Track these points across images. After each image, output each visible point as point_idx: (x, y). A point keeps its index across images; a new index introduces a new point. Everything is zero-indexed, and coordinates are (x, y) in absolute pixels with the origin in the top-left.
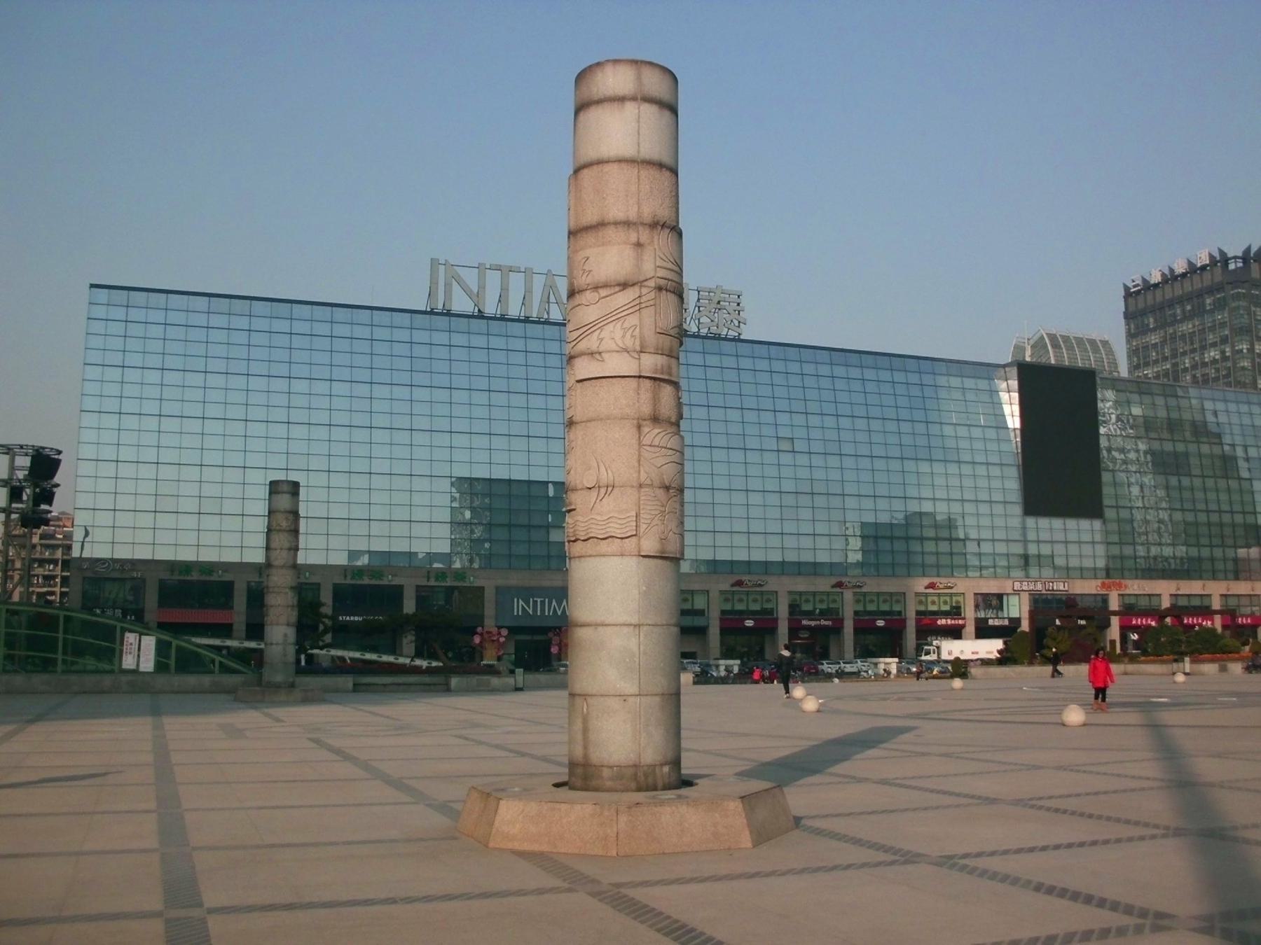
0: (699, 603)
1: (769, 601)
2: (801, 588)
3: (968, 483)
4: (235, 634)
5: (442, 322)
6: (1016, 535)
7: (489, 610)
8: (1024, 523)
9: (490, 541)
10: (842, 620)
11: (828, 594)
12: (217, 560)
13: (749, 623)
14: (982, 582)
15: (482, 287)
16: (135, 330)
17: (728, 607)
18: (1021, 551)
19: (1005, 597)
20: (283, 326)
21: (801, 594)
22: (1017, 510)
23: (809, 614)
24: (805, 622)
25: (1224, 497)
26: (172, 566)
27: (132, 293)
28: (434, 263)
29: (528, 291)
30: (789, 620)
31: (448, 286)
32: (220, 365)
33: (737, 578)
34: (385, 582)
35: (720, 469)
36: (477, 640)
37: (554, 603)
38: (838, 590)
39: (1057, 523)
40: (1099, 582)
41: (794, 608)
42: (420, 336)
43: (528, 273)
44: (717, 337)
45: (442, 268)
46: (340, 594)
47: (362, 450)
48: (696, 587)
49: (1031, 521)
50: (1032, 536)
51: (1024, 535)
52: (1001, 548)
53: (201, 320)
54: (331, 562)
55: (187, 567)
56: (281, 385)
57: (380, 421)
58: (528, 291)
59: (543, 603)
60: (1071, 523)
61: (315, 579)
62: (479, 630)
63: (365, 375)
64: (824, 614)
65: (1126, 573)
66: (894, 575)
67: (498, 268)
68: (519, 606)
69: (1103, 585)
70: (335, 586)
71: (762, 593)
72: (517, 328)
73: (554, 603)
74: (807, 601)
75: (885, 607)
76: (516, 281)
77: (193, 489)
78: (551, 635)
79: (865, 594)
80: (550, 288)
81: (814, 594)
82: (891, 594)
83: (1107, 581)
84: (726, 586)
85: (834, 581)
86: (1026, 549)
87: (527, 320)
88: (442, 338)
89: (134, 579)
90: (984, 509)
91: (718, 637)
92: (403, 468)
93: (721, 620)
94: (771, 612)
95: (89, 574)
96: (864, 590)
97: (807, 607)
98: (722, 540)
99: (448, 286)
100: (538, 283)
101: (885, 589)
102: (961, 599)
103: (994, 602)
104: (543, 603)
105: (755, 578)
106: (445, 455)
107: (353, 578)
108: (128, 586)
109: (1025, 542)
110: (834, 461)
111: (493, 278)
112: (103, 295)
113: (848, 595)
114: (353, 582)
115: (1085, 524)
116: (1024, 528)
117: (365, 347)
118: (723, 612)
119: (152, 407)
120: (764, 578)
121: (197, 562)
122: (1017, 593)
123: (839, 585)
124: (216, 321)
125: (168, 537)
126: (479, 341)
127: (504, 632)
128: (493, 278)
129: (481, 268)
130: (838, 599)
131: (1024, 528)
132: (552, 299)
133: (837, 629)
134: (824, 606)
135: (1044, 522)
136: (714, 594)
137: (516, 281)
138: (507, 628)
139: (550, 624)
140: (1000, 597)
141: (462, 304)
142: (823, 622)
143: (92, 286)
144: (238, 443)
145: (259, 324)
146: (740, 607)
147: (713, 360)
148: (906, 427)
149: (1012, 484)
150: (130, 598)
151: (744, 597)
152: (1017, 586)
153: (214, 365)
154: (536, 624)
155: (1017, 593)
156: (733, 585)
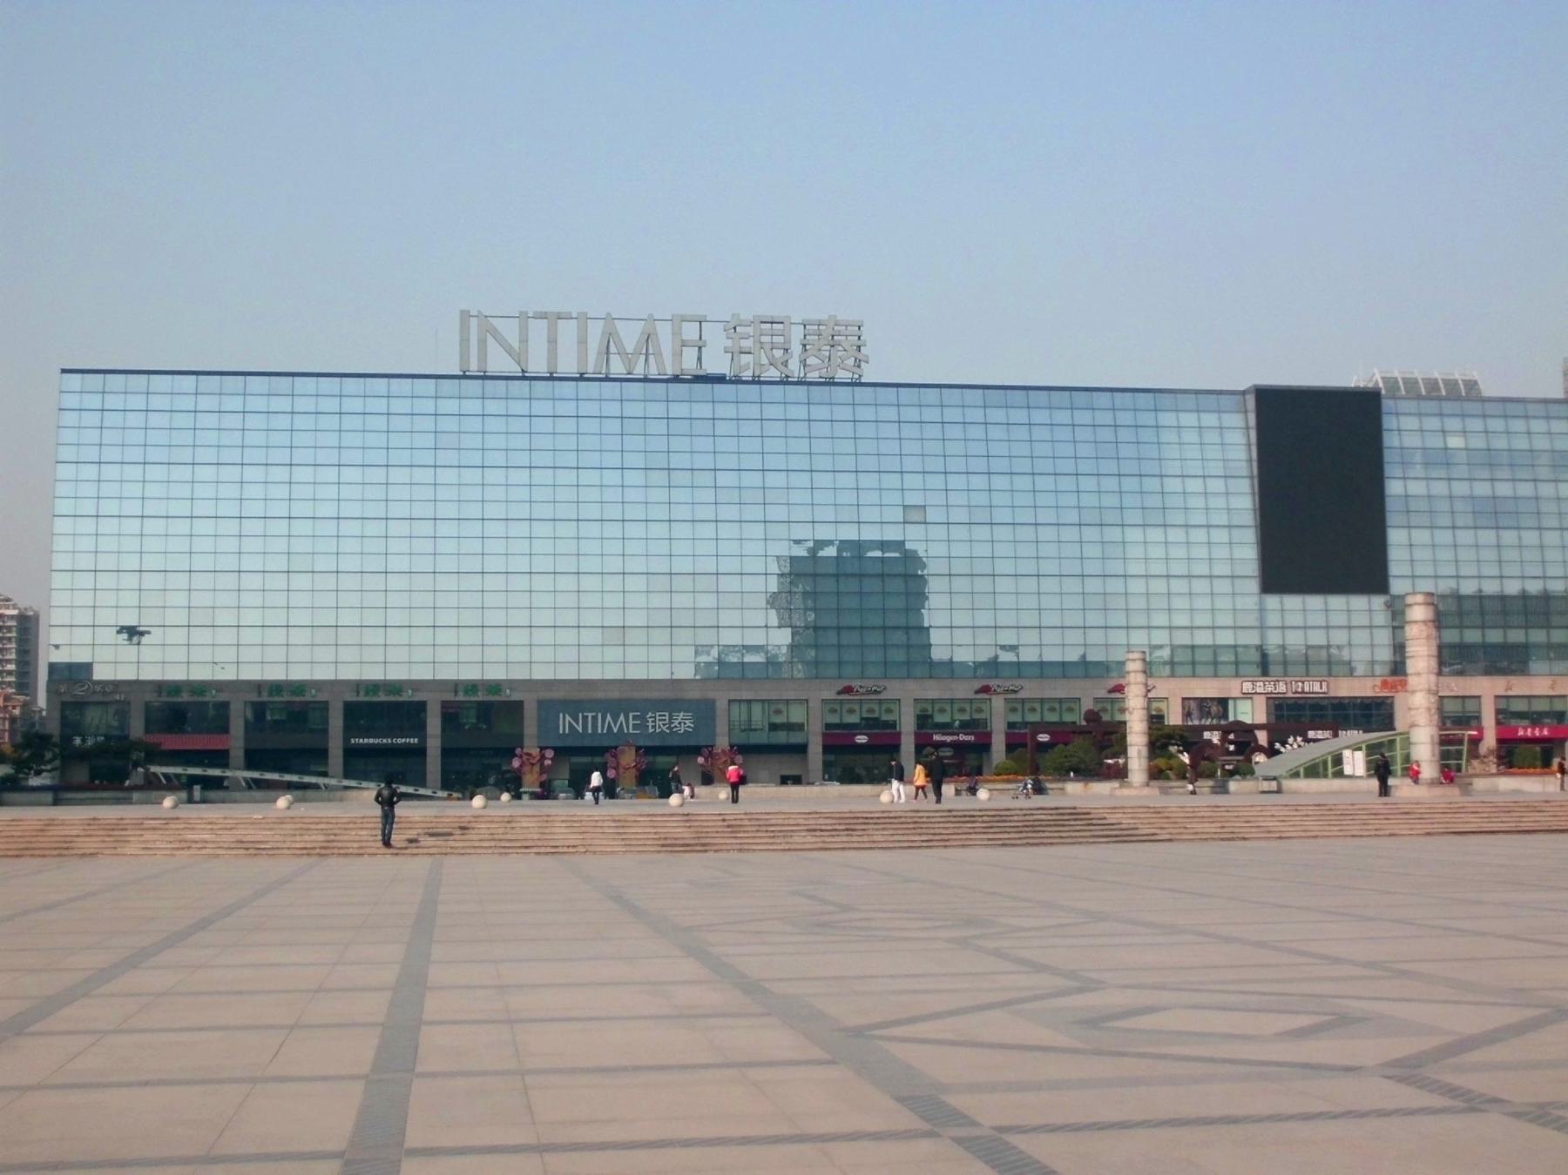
0: (797, 715)
1: (889, 711)
2: (932, 695)
3: (1179, 552)
4: (232, 762)
5: (473, 387)
6: (1252, 620)
7: (530, 728)
8: (1261, 603)
9: (816, 646)
10: (989, 735)
11: (971, 701)
12: (283, 678)
13: (862, 739)
14: (1194, 682)
15: (524, 340)
16: (111, 420)
17: (834, 719)
18: (1257, 642)
19: (1231, 703)
20: (283, 404)
21: (933, 701)
22: (1253, 586)
23: (945, 728)
24: (936, 738)
25: (1445, 555)
26: (160, 686)
27: (130, 377)
28: (465, 316)
29: (583, 341)
30: (916, 734)
31: (482, 343)
32: (498, 458)
33: (846, 683)
34: (308, 698)
35: (1049, 550)
36: (516, 763)
37: (609, 718)
38: (986, 696)
39: (1315, 601)
40: (1378, 681)
41: (923, 720)
42: (449, 406)
43: (583, 319)
44: (830, 383)
45: (474, 321)
46: (351, 710)
47: (1029, 550)
48: (791, 695)
49: (1273, 601)
50: (1273, 619)
51: (1262, 618)
52: (1226, 638)
53: (428, 406)
54: (341, 677)
55: (175, 687)
56: (280, 474)
57: (204, 508)
58: (583, 341)
59: (595, 718)
60: (1337, 602)
61: (321, 697)
62: (518, 751)
63: (980, 465)
64: (966, 726)
65: (1199, 669)
66: (1194, 676)
67: (543, 316)
68: (565, 722)
69: (1385, 684)
70: (147, 705)
71: (880, 702)
72: (567, 389)
73: (609, 718)
74: (942, 711)
75: (1052, 717)
76: (568, 331)
77: (180, 599)
78: (607, 756)
79: (1023, 701)
80: (610, 337)
81: (952, 701)
82: (1060, 701)
83: (1390, 679)
84: (830, 694)
85: (977, 685)
86: (1263, 637)
87: (646, 380)
88: (473, 406)
89: (117, 702)
90: (1200, 586)
91: (341, 760)
92: (426, 564)
93: (825, 736)
94: (893, 725)
95: (66, 699)
96: (1022, 695)
97: (940, 719)
98: (1051, 637)
99: (482, 343)
100: (595, 331)
101: (1049, 693)
102: (1163, 706)
103: (1214, 709)
104: (595, 718)
105: (869, 683)
106: (476, 546)
107: (367, 694)
108: (111, 710)
109: (1262, 628)
110: (982, 533)
111: (538, 329)
112: (75, 381)
113: (998, 703)
114: (367, 699)
115: (1359, 602)
116: (1262, 610)
117: (801, 429)
118: (828, 726)
119: (133, 508)
120: (882, 683)
121: (434, 681)
122: (1248, 696)
123: (986, 689)
124: (205, 403)
125: (402, 654)
126: (520, 407)
127: (550, 754)
128: (538, 329)
129: (523, 318)
130: (984, 706)
131: (1262, 610)
132: (613, 349)
133: (984, 746)
134: (966, 717)
135: (1293, 602)
136: (815, 704)
137: (568, 331)
138: (555, 749)
139: (606, 744)
140: (1223, 702)
141: (500, 362)
142: (962, 737)
143: (64, 371)
144: (616, 547)
145: (256, 403)
146: (1033, 718)
147: (820, 412)
148: (1088, 483)
149: (1247, 552)
150: (115, 724)
151: (856, 707)
152: (1247, 687)
153: (587, 459)
154: (587, 743)
155: (1248, 696)
156: (977, 692)
